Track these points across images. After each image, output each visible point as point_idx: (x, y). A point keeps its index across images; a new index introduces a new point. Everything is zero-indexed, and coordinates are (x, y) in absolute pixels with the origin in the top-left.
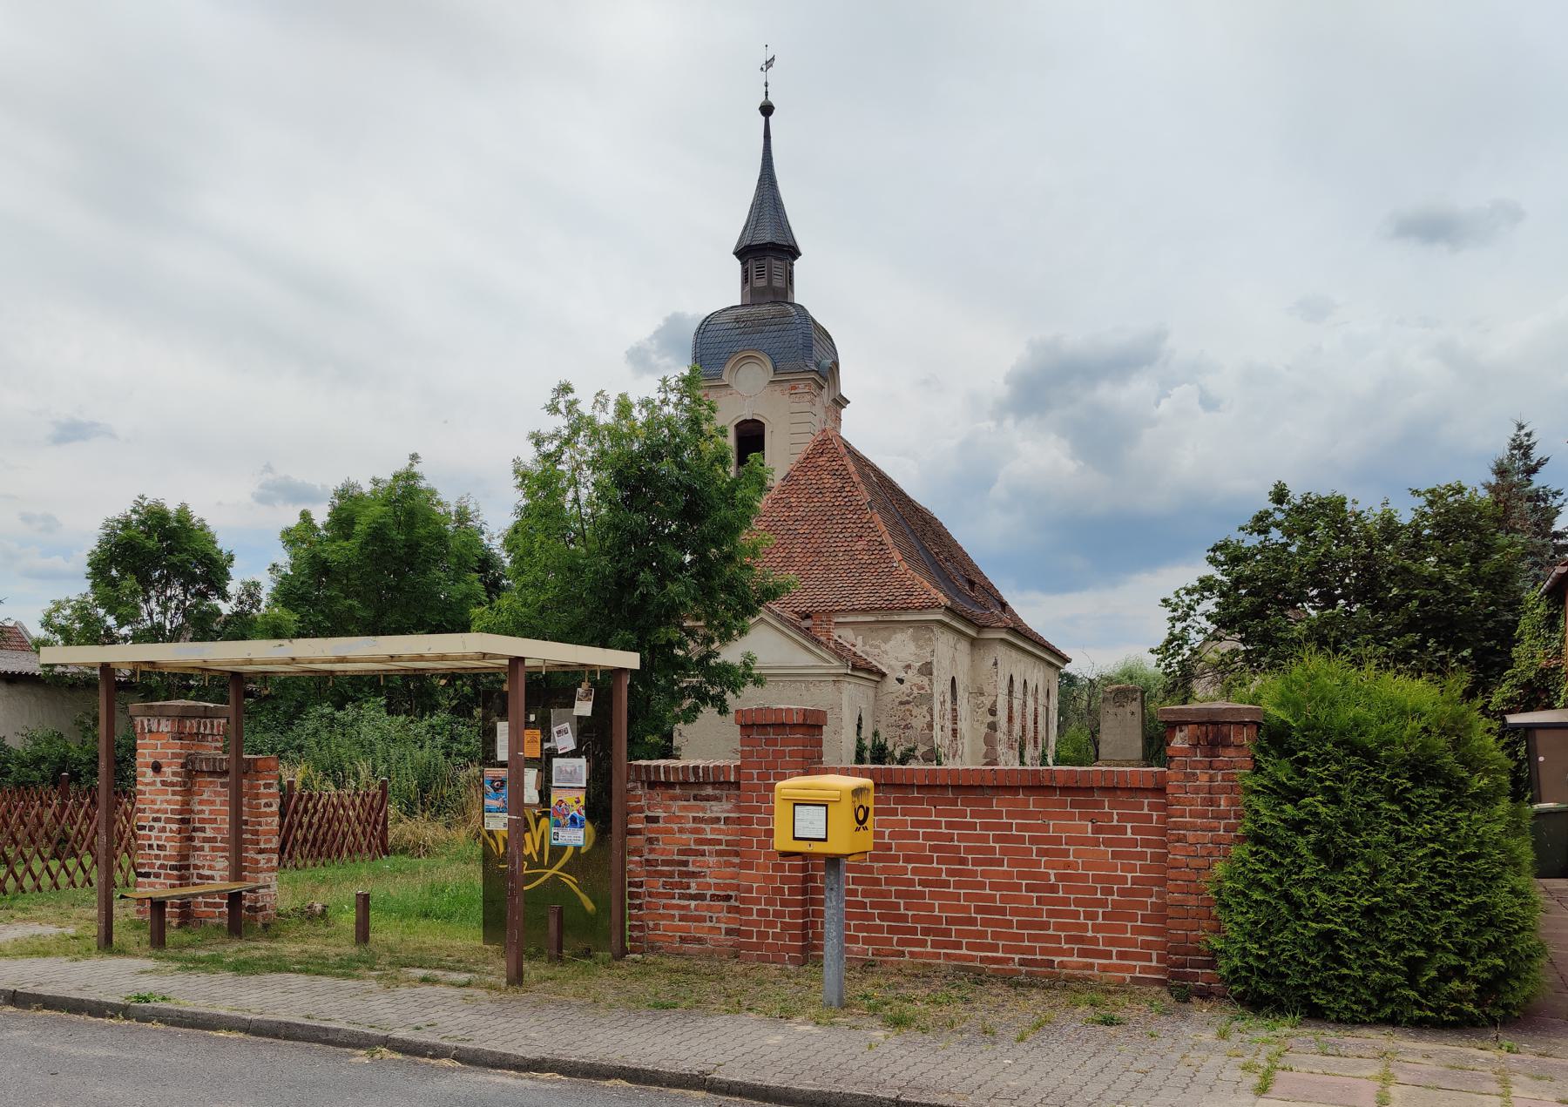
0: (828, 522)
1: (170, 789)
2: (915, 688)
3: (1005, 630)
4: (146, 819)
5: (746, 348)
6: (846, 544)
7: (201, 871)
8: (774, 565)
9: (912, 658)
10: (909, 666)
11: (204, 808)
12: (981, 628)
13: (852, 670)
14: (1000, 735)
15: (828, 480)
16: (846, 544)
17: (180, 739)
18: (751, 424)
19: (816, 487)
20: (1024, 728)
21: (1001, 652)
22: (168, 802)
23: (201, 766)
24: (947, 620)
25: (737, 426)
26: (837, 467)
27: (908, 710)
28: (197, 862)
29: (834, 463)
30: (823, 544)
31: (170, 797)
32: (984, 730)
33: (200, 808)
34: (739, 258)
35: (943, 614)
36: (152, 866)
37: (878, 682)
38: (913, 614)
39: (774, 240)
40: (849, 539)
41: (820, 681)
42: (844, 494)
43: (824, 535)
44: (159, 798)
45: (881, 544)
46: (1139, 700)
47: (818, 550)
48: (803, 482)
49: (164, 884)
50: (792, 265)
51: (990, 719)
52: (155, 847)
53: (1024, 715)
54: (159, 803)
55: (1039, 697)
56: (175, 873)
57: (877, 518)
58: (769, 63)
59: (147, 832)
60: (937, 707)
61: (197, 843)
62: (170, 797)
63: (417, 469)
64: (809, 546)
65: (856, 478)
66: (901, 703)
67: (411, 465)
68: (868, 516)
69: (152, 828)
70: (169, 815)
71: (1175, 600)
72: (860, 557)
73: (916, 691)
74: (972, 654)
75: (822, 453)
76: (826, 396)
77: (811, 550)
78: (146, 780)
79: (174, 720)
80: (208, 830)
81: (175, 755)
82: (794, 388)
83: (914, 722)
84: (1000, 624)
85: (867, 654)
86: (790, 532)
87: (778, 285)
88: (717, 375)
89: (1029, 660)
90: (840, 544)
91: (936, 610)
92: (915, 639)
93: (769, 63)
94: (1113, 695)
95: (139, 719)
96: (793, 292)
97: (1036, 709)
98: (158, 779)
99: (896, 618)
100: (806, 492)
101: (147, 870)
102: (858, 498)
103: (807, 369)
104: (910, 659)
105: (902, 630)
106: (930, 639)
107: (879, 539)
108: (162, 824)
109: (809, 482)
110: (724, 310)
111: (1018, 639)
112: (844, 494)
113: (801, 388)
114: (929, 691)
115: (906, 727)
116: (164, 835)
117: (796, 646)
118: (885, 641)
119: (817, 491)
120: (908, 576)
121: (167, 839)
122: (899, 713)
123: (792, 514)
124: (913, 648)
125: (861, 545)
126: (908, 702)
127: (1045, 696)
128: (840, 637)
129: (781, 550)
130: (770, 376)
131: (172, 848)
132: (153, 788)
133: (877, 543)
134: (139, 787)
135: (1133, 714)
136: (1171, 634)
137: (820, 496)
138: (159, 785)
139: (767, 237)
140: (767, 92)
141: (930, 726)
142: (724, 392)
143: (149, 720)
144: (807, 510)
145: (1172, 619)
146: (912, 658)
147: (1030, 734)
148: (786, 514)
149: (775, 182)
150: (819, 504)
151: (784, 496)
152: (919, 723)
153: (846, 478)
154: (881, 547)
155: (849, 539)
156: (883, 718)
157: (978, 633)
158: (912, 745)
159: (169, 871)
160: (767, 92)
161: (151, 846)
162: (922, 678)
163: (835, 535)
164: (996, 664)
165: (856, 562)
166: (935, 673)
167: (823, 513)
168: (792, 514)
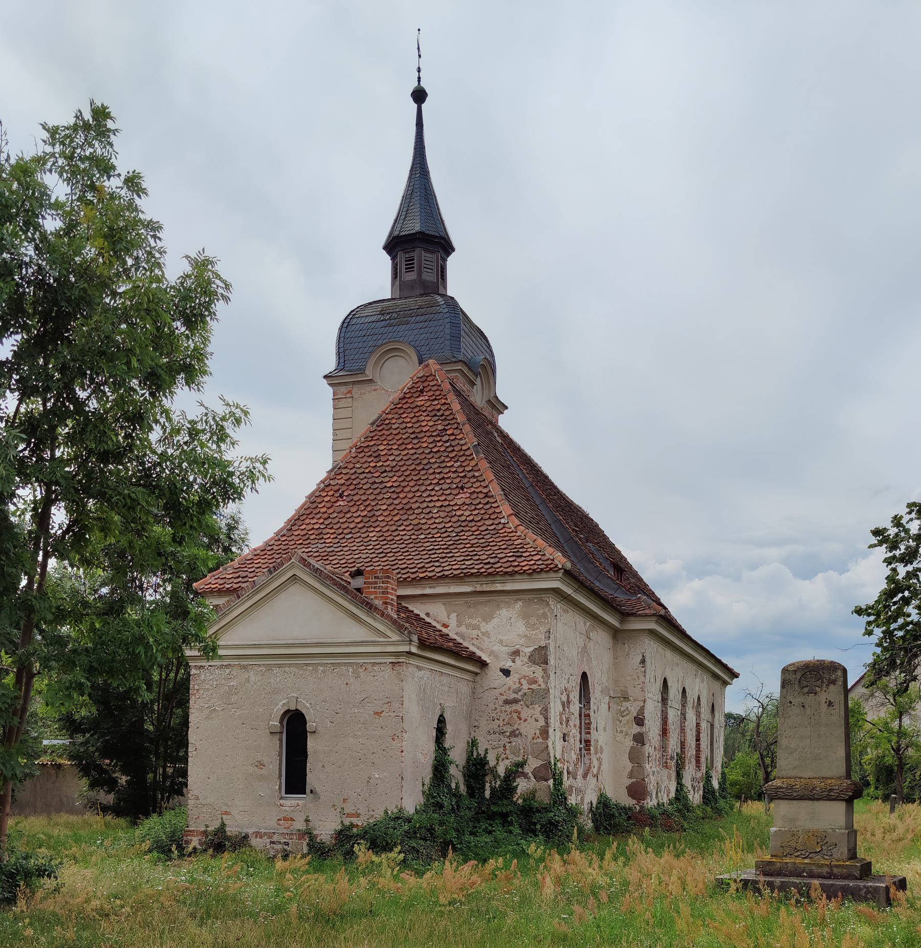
0: (423, 472)
2: (524, 682)
3: (655, 619)
6: (443, 498)
8: (352, 526)
9: (522, 641)
10: (516, 653)
12: (625, 615)
13: (419, 648)
14: (648, 749)
15: (427, 423)
16: (443, 498)
19: (410, 431)
20: (683, 744)
21: (650, 647)
24: (569, 591)
26: (439, 407)
27: (516, 711)
29: (436, 402)
30: (414, 500)
32: (629, 743)
34: (389, 253)
35: (561, 580)
37: (476, 674)
38: (522, 581)
39: (423, 230)
40: (448, 492)
41: (374, 664)
42: (445, 438)
43: (416, 488)
46: (840, 683)
47: (407, 507)
48: (397, 425)
50: (445, 260)
51: (636, 729)
53: (683, 730)
55: (702, 710)
57: (484, 465)
60: (555, 708)
64: (396, 502)
65: (461, 418)
66: (507, 702)
68: (473, 463)
71: (892, 531)
72: (458, 513)
73: (525, 686)
74: (614, 645)
75: (422, 391)
77: (399, 507)
84: (647, 611)
85: (463, 637)
86: (375, 486)
87: (428, 278)
89: (691, 667)
90: (435, 498)
91: (552, 575)
92: (525, 616)
94: (798, 676)
97: (698, 725)
99: (499, 587)
100: (398, 437)
102: (462, 442)
103: (454, 360)
106: (545, 616)
109: (404, 425)
110: (370, 304)
111: (672, 634)
112: (445, 438)
114: (543, 686)
115: (513, 734)
117: (340, 614)
118: (487, 618)
119: (412, 436)
120: (519, 533)
122: (503, 716)
123: (379, 464)
124: (523, 628)
125: (462, 498)
126: (516, 701)
127: (709, 710)
128: (428, 615)
129: (362, 508)
133: (481, 496)
135: (830, 704)
136: (891, 579)
137: (415, 441)
139: (415, 226)
140: (419, 78)
141: (545, 733)
142: (368, 388)
144: (398, 459)
145: (888, 561)
146: (522, 641)
147: (691, 752)
148: (372, 464)
150: (413, 451)
151: (372, 443)
152: (530, 728)
153: (448, 418)
154: (487, 500)
155: (448, 492)
156: (483, 723)
157: (622, 622)
158: (520, 759)
160: (419, 78)
162: (535, 668)
163: (430, 488)
164: (643, 661)
165: (454, 519)
166: (552, 661)
167: (418, 461)
168: (379, 464)
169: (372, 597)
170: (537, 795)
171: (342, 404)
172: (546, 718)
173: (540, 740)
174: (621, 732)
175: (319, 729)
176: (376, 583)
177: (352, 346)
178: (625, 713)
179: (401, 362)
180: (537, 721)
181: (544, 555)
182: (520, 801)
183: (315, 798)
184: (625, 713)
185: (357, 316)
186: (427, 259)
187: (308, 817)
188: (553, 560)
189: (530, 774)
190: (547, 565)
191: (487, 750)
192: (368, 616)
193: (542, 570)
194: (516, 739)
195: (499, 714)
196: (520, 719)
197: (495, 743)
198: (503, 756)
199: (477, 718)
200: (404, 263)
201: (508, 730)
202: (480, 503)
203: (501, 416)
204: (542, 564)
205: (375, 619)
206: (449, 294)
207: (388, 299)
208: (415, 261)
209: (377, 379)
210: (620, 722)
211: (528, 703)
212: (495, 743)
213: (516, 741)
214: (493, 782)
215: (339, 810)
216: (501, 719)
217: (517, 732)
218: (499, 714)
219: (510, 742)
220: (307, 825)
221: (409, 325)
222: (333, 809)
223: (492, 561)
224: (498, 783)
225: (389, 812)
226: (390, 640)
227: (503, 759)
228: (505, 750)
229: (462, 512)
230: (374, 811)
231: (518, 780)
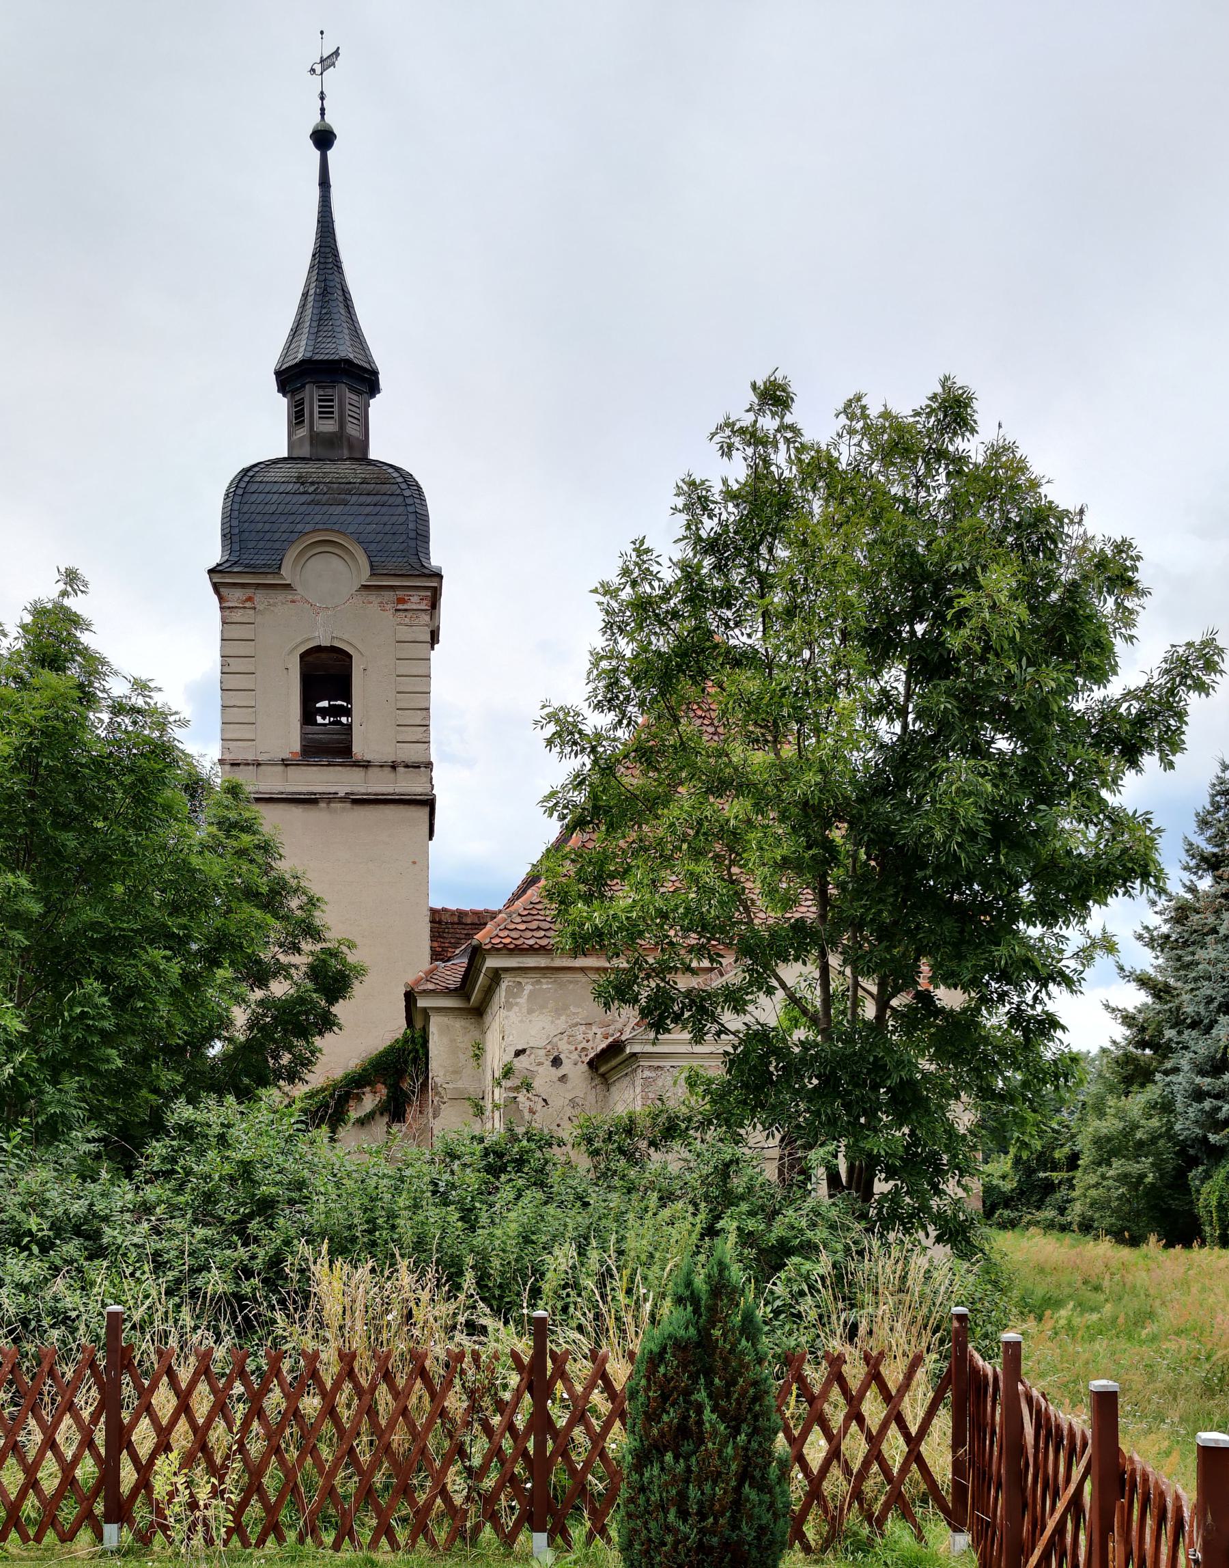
18: (324, 655)
25: (302, 656)
39: (351, 356)
58: (328, 61)
63: (74, 603)
67: (64, 594)
82: (401, 601)
88: (270, 566)
93: (328, 61)
140: (323, 110)
142: (281, 596)
160: (323, 110)
171: (237, 616)
177: (252, 526)
179: (336, 563)
206: (372, 455)
207: (285, 459)
208: (336, 403)
209: (296, 585)
221: (348, 508)
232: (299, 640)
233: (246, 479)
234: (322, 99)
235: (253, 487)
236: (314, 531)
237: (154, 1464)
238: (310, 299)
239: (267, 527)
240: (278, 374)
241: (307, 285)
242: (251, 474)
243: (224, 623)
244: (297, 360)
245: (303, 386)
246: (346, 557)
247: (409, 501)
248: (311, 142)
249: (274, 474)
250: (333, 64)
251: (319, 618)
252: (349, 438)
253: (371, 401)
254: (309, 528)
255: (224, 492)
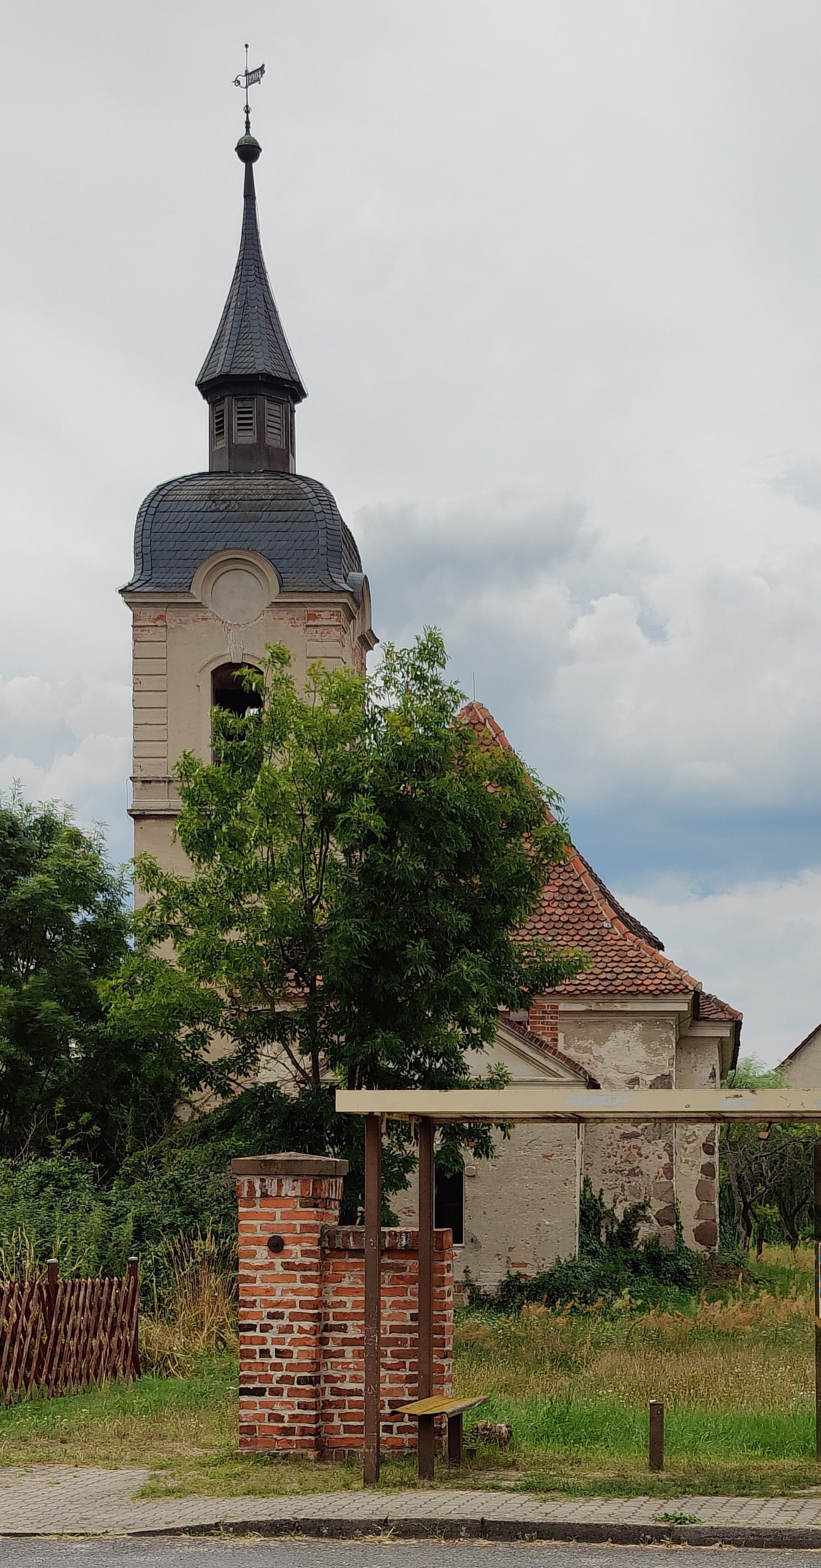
1: (298, 1274)
4: (259, 1316)
5: (230, 544)
7: (338, 1385)
9: (642, 1068)
11: (344, 1299)
17: (316, 1206)
22: (295, 1292)
23: (345, 1243)
25: (214, 673)
27: (635, 1147)
28: (330, 1372)
31: (298, 1285)
33: (337, 1299)
34: (205, 395)
36: (269, 1379)
39: (269, 370)
44: (279, 1287)
45: (580, 891)
49: (288, 1403)
52: (272, 1353)
54: (278, 1293)
56: (308, 1387)
58: (254, 76)
59: (258, 1333)
61: (331, 1347)
62: (298, 1285)
69: (265, 1328)
70: (297, 1310)
72: (549, 910)
76: (355, 630)
78: (256, 1263)
79: (305, 1181)
80: (350, 1329)
81: (305, 1228)
82: (312, 616)
83: (644, 1166)
84: (722, 1015)
88: (180, 585)
91: (681, 997)
92: (646, 1040)
93: (254, 76)
95: (244, 1179)
96: (294, 456)
98: (278, 1261)
99: (618, 1007)
101: (257, 1385)
104: (638, 1070)
105: (626, 1026)
107: (577, 884)
108: (285, 1322)
113: (325, 617)
115: (633, 1173)
116: (288, 1337)
118: (601, 1041)
120: (629, 942)
121: (294, 1342)
122: (620, 1152)
124: (644, 1053)
130: (273, 592)
131: (301, 1355)
132: (269, 1273)
133: (574, 891)
134: (242, 1272)
138: (279, 1269)
140: (248, 123)
142: (192, 614)
143: (263, 1180)
146: (642, 1068)
149: (264, 273)
152: (652, 1166)
154: (581, 896)
156: (597, 1159)
158: (641, 1200)
159: (296, 1386)
160: (248, 123)
161: (265, 1353)
169: (540, 1033)
170: (661, 1241)
171: (148, 635)
172: (671, 1156)
173: (664, 1180)
174: (687, 1162)
175: (479, 1173)
176: (544, 1018)
178: (691, 1140)
180: (660, 1158)
181: (668, 972)
182: (642, 1248)
183: (475, 1247)
184: (691, 1140)
185: (172, 498)
186: (271, 412)
187: (467, 1267)
188: (681, 980)
189: (653, 1218)
190: (676, 986)
191: (602, 1190)
192: (538, 1053)
193: (671, 991)
194: (636, 1179)
195: (616, 1150)
196: (641, 1156)
197: (611, 1183)
198: (621, 1197)
199: (590, 1154)
200: (235, 416)
201: (627, 1168)
202: (573, 900)
203: (370, 652)
204: (670, 984)
205: (545, 1057)
210: (686, 1149)
211: (650, 1138)
212: (611, 1183)
213: (636, 1181)
214: (610, 1228)
215: (504, 1259)
216: (618, 1156)
217: (637, 1171)
218: (616, 1150)
219: (629, 1182)
220: (467, 1276)
222: (496, 1258)
223: (609, 976)
224: (616, 1228)
225: (562, 1261)
226: (561, 1079)
227: (621, 1201)
228: (623, 1190)
229: (553, 910)
230: (544, 1260)
231: (639, 1224)
232: (210, 657)
233: (159, 498)
234: (247, 112)
235: (165, 506)
236: (225, 549)
237: (699, 1003)
238: (231, 312)
239: (179, 545)
240: (200, 385)
241: (230, 297)
242: (163, 492)
243: (135, 641)
244: (216, 375)
245: (223, 398)
246: (257, 575)
247: (320, 517)
248: (236, 154)
249: (187, 493)
250: (259, 80)
251: (230, 635)
252: (268, 449)
253: (297, 407)
254: (220, 546)
255: (137, 510)
